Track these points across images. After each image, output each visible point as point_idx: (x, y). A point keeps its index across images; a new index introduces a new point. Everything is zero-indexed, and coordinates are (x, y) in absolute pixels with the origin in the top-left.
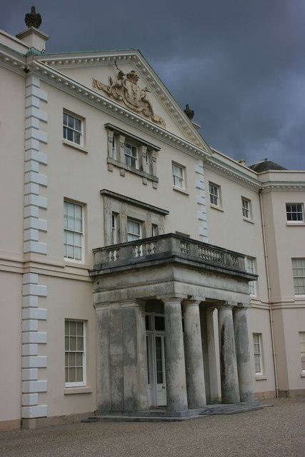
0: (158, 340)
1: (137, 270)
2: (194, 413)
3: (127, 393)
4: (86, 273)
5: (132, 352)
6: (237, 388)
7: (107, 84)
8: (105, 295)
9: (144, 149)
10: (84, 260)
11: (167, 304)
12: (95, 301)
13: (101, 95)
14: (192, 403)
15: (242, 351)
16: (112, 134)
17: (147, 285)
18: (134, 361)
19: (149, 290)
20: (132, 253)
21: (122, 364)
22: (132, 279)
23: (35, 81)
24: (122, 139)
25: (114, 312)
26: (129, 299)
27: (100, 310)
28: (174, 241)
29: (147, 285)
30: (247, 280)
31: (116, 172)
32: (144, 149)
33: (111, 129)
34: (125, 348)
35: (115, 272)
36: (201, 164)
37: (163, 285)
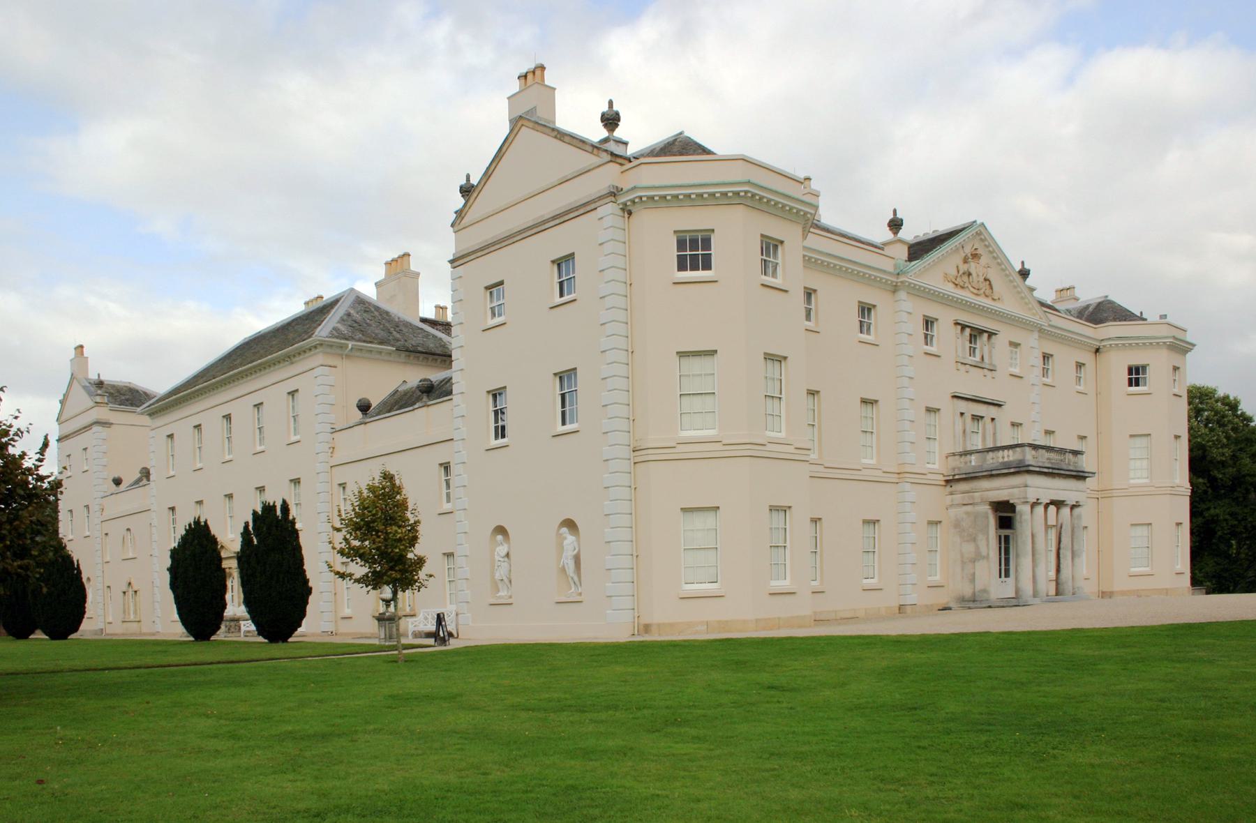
0: (1007, 538)
1: (992, 476)
2: (1037, 600)
3: (979, 586)
4: (941, 478)
5: (984, 551)
6: (1070, 583)
7: (954, 272)
8: (958, 498)
9: (986, 335)
10: (938, 465)
11: (1018, 508)
12: (949, 503)
13: (949, 289)
14: (1035, 595)
15: (1076, 547)
16: (959, 327)
17: (1002, 489)
18: (987, 557)
19: (1002, 496)
20: (985, 460)
21: (973, 561)
22: (985, 484)
23: (902, 295)
24: (968, 331)
25: (967, 513)
26: (983, 502)
27: (952, 512)
28: (1027, 449)
29: (1002, 489)
30: (1084, 478)
31: (962, 368)
32: (986, 335)
33: (964, 327)
34: (977, 548)
35: (970, 478)
36: (1036, 335)
37: (1015, 491)
